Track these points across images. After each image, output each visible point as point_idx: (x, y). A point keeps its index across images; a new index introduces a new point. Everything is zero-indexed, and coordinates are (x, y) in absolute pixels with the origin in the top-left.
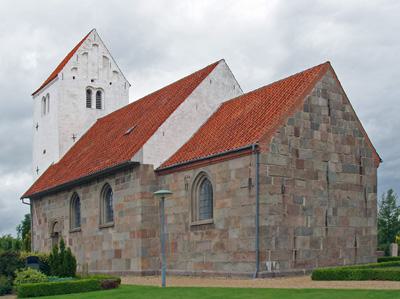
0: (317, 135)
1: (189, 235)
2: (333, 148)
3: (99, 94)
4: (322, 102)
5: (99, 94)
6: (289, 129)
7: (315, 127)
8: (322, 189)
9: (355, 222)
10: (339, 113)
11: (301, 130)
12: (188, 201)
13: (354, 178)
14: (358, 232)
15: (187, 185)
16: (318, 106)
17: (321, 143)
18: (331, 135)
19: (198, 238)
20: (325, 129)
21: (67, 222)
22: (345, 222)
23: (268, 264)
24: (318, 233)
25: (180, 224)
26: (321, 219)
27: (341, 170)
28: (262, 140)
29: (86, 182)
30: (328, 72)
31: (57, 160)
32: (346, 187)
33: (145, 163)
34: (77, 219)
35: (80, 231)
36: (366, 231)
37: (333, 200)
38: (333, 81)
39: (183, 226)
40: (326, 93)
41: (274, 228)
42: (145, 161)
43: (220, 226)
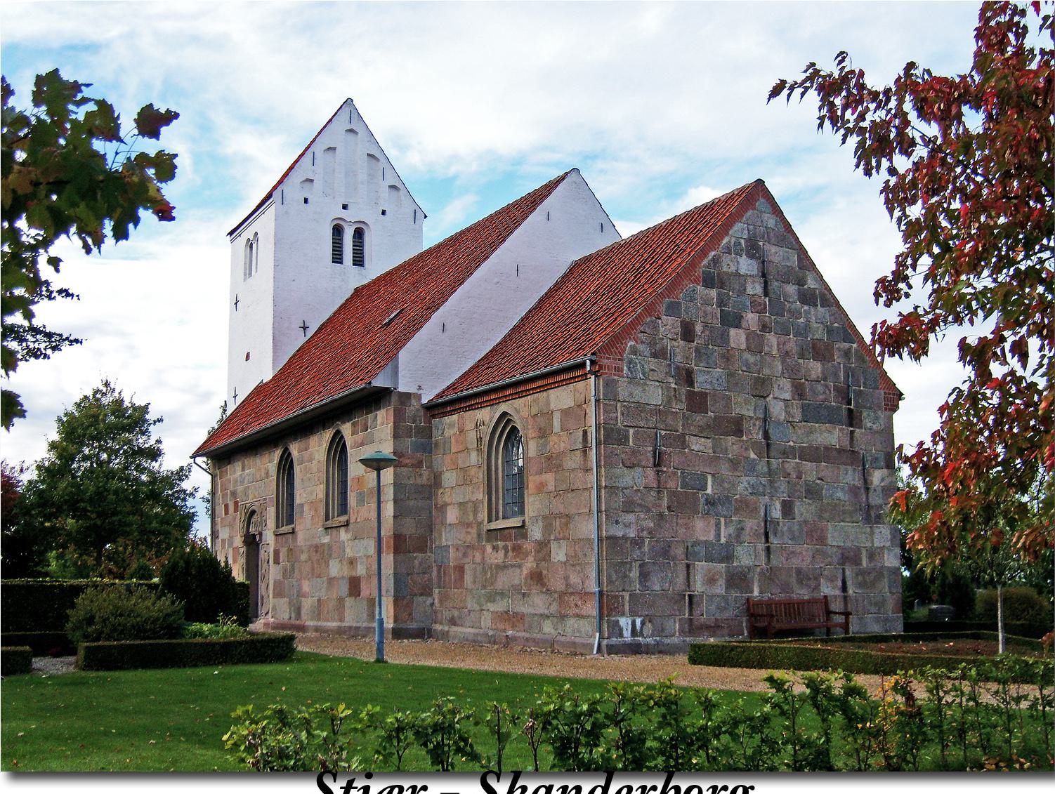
0: (737, 338)
1: (484, 551)
2: (779, 367)
3: (359, 234)
4: (746, 266)
5: (359, 234)
6: (668, 325)
7: (732, 320)
8: (753, 456)
9: (839, 534)
10: (791, 289)
11: (698, 328)
12: (481, 475)
13: (832, 436)
14: (849, 557)
15: (480, 440)
16: (737, 274)
17: (747, 356)
18: (772, 339)
19: (499, 558)
20: (754, 327)
21: (271, 512)
22: (816, 535)
23: (625, 622)
24: (745, 557)
25: (468, 525)
26: (752, 524)
27: (798, 417)
28: (606, 349)
29: (304, 427)
30: (761, 203)
31: (268, 376)
32: (813, 454)
33: (401, 389)
34: (287, 511)
35: (293, 532)
36: (871, 556)
37: (782, 485)
38: (771, 221)
39: (474, 531)
40: (757, 248)
41: (637, 543)
42: (404, 385)
43: (536, 533)
